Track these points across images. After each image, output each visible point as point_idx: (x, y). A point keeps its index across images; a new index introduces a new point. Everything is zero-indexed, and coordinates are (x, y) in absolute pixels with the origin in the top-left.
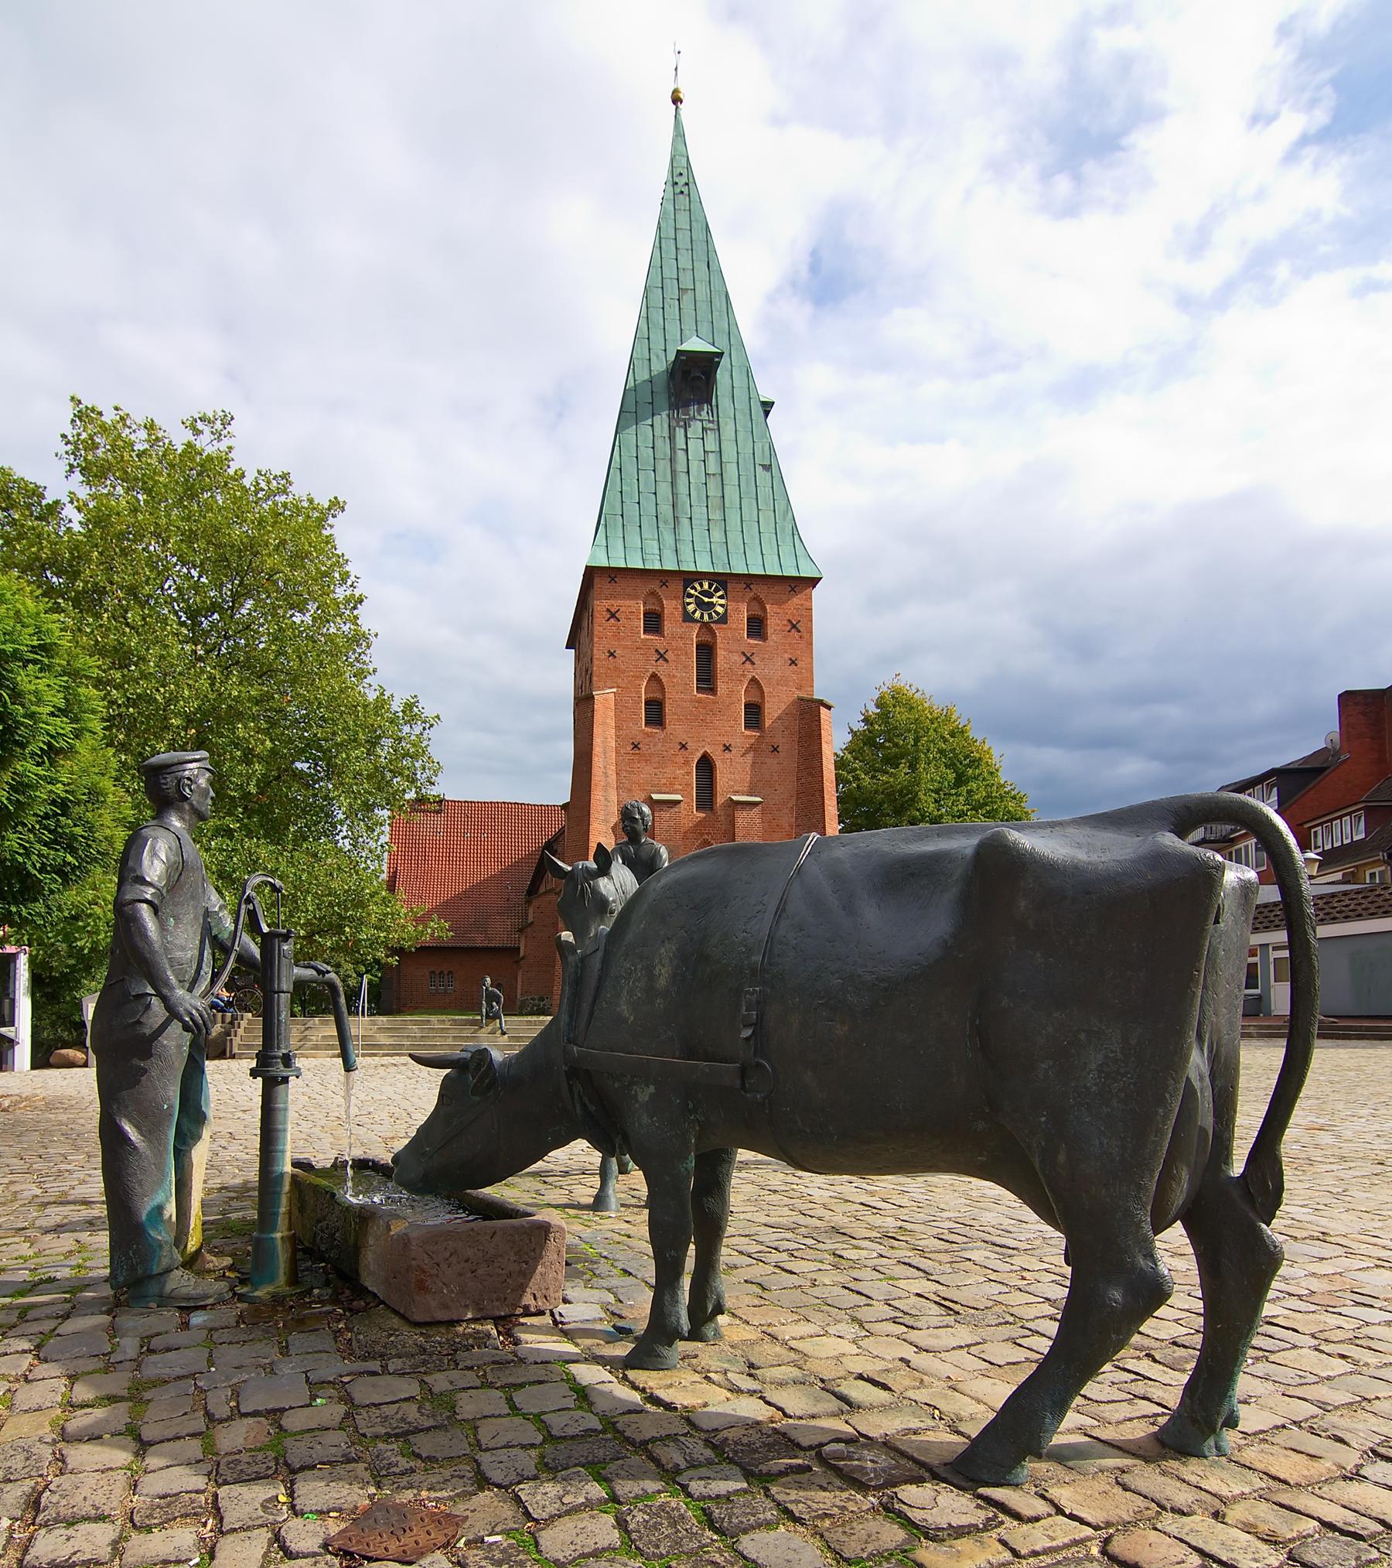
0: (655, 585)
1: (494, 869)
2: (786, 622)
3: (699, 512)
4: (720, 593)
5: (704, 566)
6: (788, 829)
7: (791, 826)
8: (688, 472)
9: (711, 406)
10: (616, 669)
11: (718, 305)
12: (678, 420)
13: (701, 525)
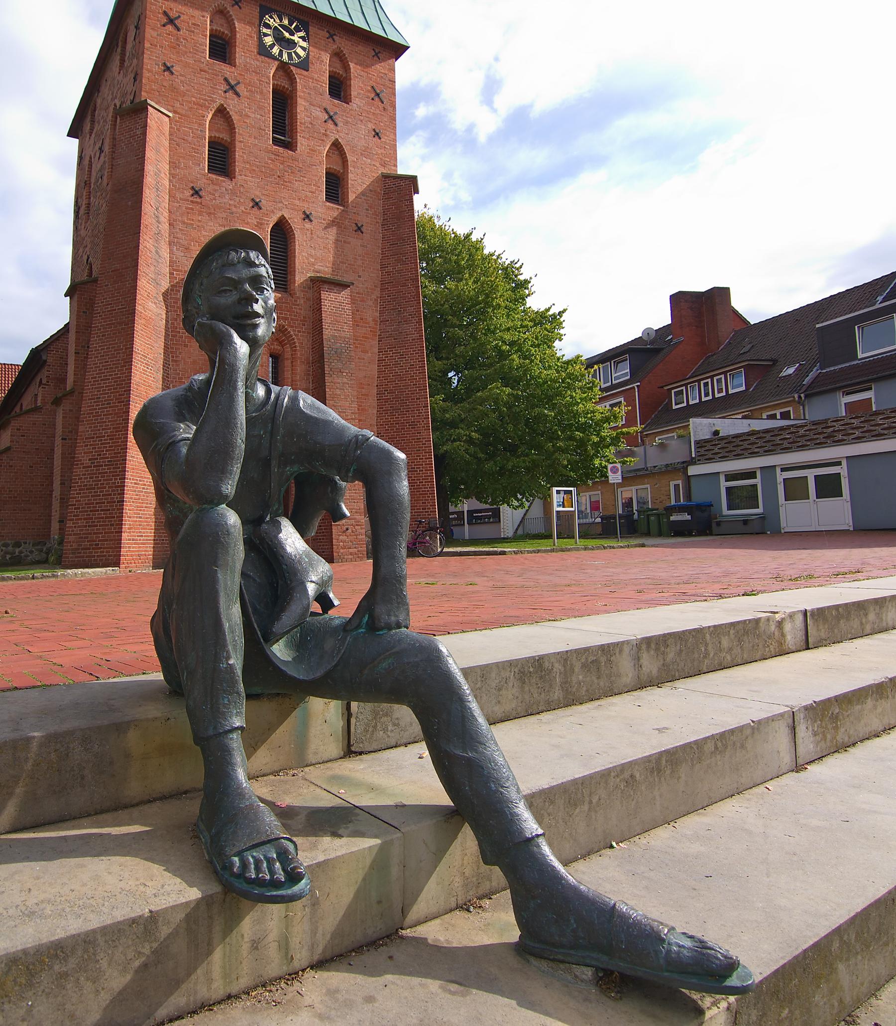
6: (372, 324)
7: (374, 320)
10: (173, 89)
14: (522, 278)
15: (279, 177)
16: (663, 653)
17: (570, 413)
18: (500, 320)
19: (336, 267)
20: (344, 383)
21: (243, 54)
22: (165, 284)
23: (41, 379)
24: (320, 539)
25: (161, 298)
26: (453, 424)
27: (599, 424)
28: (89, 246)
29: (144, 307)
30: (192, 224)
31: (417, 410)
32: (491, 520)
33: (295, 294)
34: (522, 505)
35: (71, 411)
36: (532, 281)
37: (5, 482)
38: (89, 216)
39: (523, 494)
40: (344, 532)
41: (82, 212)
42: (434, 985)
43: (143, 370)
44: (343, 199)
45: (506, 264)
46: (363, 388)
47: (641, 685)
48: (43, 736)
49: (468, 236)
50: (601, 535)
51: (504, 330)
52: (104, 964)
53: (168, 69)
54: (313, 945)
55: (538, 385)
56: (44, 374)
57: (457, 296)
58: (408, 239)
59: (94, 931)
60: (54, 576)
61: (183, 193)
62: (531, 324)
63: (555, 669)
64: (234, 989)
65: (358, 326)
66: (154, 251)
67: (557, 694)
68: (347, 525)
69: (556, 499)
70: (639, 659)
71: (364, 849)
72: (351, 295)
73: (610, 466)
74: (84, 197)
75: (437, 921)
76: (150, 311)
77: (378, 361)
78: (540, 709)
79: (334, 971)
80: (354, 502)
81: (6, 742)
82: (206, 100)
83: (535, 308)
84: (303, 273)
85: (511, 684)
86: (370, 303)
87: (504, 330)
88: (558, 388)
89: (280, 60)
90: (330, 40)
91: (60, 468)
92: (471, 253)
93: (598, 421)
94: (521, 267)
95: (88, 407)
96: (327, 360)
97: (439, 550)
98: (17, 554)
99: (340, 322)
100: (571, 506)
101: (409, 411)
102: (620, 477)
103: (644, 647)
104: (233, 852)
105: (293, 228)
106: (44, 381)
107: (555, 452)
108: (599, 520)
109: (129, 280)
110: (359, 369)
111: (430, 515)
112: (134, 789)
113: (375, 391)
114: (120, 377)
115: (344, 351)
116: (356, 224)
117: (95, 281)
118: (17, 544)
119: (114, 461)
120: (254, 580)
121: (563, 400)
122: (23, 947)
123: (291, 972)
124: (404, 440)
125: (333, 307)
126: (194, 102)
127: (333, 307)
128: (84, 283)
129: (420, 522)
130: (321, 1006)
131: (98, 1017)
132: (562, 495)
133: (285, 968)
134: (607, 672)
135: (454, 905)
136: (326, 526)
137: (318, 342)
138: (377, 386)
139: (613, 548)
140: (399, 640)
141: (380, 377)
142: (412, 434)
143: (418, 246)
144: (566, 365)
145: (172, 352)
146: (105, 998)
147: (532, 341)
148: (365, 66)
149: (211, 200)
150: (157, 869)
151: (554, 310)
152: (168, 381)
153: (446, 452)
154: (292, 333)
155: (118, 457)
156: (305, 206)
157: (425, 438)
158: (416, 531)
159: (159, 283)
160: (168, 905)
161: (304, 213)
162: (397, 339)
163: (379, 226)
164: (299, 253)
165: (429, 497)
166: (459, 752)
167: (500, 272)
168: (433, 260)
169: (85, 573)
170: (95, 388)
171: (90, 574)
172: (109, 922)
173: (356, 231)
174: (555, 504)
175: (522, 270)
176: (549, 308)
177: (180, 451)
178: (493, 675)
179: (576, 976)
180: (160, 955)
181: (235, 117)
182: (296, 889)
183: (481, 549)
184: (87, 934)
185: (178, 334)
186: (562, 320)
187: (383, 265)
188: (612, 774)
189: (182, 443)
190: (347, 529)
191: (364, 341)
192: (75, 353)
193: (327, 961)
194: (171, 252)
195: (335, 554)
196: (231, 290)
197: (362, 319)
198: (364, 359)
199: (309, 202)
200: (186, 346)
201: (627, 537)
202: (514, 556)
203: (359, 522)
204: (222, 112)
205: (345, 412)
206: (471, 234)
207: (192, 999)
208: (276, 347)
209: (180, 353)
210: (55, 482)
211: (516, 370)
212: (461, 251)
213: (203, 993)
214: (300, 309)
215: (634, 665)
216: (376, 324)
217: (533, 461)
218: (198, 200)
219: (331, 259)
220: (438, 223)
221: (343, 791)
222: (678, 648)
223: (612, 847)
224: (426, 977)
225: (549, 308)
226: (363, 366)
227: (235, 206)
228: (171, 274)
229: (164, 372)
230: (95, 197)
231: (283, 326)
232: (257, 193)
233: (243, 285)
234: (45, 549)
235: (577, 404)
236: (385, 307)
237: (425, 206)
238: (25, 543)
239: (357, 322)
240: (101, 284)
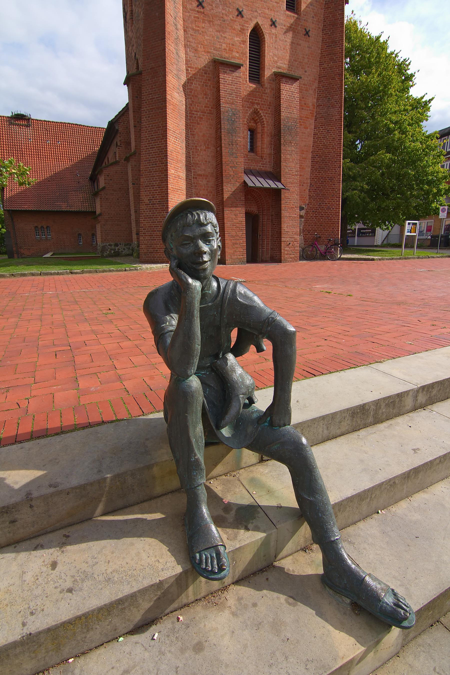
1: (67, 164)
6: (311, 107)
7: (313, 105)
14: (409, 72)
16: (430, 392)
17: (425, 172)
18: (391, 106)
19: (291, 64)
20: (292, 151)
22: (184, 79)
23: (117, 142)
24: (275, 249)
25: (182, 89)
26: (354, 178)
27: (439, 180)
28: (135, 45)
29: (171, 96)
30: (198, 31)
31: (334, 170)
32: (370, 235)
33: (264, 85)
34: (388, 228)
35: (135, 166)
36: (416, 75)
37: (105, 208)
38: (133, 21)
39: (389, 222)
40: (288, 245)
41: (128, 17)
42: (283, 598)
43: (174, 141)
44: (297, 9)
45: (401, 62)
46: (303, 154)
47: (415, 409)
48: (112, 476)
49: (378, 38)
50: (429, 246)
51: (393, 113)
52: (141, 601)
54: (233, 577)
55: (408, 153)
56: (118, 139)
57: (366, 86)
58: (338, 42)
59: (135, 592)
61: (192, 4)
62: (410, 108)
63: (371, 409)
64: (199, 597)
65: (302, 109)
66: (175, 53)
67: (370, 419)
68: (290, 241)
69: (407, 227)
70: (417, 397)
71: (258, 539)
72: (299, 87)
73: (441, 208)
74: (128, 5)
75: (291, 557)
76: (175, 99)
78: (360, 428)
79: (242, 586)
80: (294, 228)
81: (94, 481)
83: (415, 96)
84: (269, 69)
85: (346, 419)
86: (311, 92)
87: (393, 113)
88: (420, 155)
91: (133, 202)
92: (379, 52)
93: (440, 178)
94: (409, 64)
95: (145, 166)
97: (339, 256)
98: (117, 250)
99: (291, 107)
100: (414, 232)
101: (329, 170)
102: (446, 215)
103: (421, 391)
104: (196, 552)
105: (264, 33)
106: (119, 144)
107: (411, 198)
108: (429, 237)
109: (161, 76)
110: (302, 141)
111: (336, 236)
112: (158, 490)
113: (310, 156)
114: (160, 147)
115: (293, 128)
117: (141, 74)
118: (116, 245)
119: (162, 201)
120: (214, 388)
121: (422, 163)
122: (104, 603)
123: (223, 587)
124: (325, 189)
125: (288, 95)
127: (288, 95)
128: (134, 75)
129: (330, 240)
130: (234, 607)
131: (140, 618)
132: (411, 225)
133: (221, 586)
134: (398, 406)
135: (299, 548)
136: (278, 241)
137: (278, 121)
138: (312, 152)
139: (434, 257)
140: (284, 435)
141: (314, 146)
142: (330, 185)
143: (345, 46)
144: (427, 139)
145: (190, 128)
146: (142, 612)
147: (409, 121)
149: (210, 10)
150: (165, 549)
151: (426, 98)
152: (189, 148)
153: (347, 196)
154: (262, 114)
155: (163, 199)
156: (272, 14)
157: (337, 188)
158: (327, 245)
159: (180, 77)
160: (167, 577)
161: (271, 20)
162: (326, 119)
163: (320, 31)
164: (268, 53)
165: (336, 225)
166: (306, 497)
167: (396, 67)
168: (354, 57)
169: (152, 268)
170: (147, 153)
172: (141, 588)
173: (305, 35)
174: (406, 231)
175: (410, 67)
176: (424, 96)
177: (166, 341)
178: (338, 416)
179: (343, 600)
180: (165, 594)
182: (223, 573)
183: (362, 257)
184: (132, 594)
185: (193, 116)
186: (430, 105)
187: (321, 62)
188: (384, 484)
189: (168, 334)
190: (290, 244)
191: (306, 120)
192: (134, 126)
193: (240, 580)
194: (186, 54)
195: (282, 258)
196: (190, 243)
199: (275, 12)
200: (198, 124)
201: (443, 249)
202: (379, 262)
205: (292, 171)
206: (380, 36)
207: (180, 604)
208: (252, 124)
209: (195, 129)
210: (131, 210)
211: (396, 141)
212: (372, 50)
213: (185, 601)
215: (414, 400)
216: (314, 108)
217: (398, 203)
218: (202, 10)
219: (288, 58)
220: (360, 27)
221: (255, 493)
222: (439, 388)
223: (378, 513)
224: (280, 593)
225: (424, 96)
227: (226, 15)
228: (187, 70)
229: (186, 142)
230: (135, 5)
231: (257, 110)
232: (241, 4)
233: (197, 240)
234: (131, 248)
235: (430, 166)
236: (321, 96)
237: (353, 12)
238: (120, 244)
239: (302, 107)
240: (144, 78)
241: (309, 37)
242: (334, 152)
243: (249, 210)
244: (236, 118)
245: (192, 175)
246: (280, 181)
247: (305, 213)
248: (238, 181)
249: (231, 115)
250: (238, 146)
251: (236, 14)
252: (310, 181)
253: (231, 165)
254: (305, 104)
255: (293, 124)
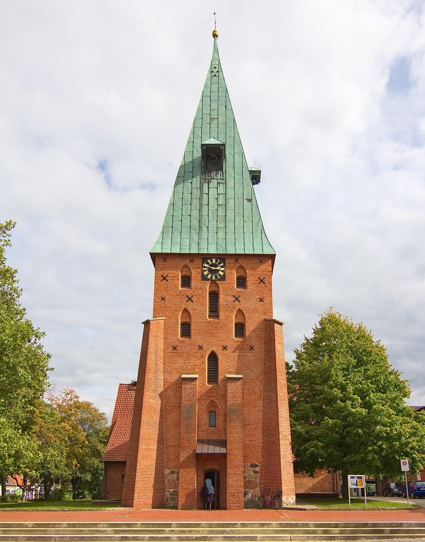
0: (187, 262)
2: (257, 279)
3: (213, 224)
4: (222, 265)
5: (212, 250)
7: (260, 391)
8: (208, 204)
9: (223, 172)
10: (165, 306)
11: (229, 124)
12: (205, 179)
13: (213, 230)
15: (211, 333)
21: (195, 282)
30: (173, 362)
40: (233, 496)
53: (163, 299)
60: (100, 510)
68: (235, 493)
77: (263, 410)
80: (239, 482)
82: (178, 308)
89: (212, 280)
90: (236, 262)
96: (228, 415)
100: (362, 485)
105: (218, 355)
115: (237, 410)
116: (250, 346)
126: (174, 310)
138: (262, 423)
148: (253, 269)
154: (217, 403)
171: (117, 510)
173: (250, 350)
181: (191, 312)
183: (300, 507)
197: (253, 391)
198: (255, 410)
200: (170, 414)
203: (241, 491)
204: (186, 310)
214: (221, 391)
226: (254, 414)
227: (191, 351)
231: (213, 400)
241: (253, 350)
242: (274, 423)
243: (212, 468)
244: (192, 409)
245: (165, 446)
246: (226, 447)
247: (260, 469)
248: (191, 449)
249: (188, 408)
250: (192, 427)
251: (198, 348)
252: (262, 444)
253: (186, 439)
254: (253, 391)
255: (237, 407)
